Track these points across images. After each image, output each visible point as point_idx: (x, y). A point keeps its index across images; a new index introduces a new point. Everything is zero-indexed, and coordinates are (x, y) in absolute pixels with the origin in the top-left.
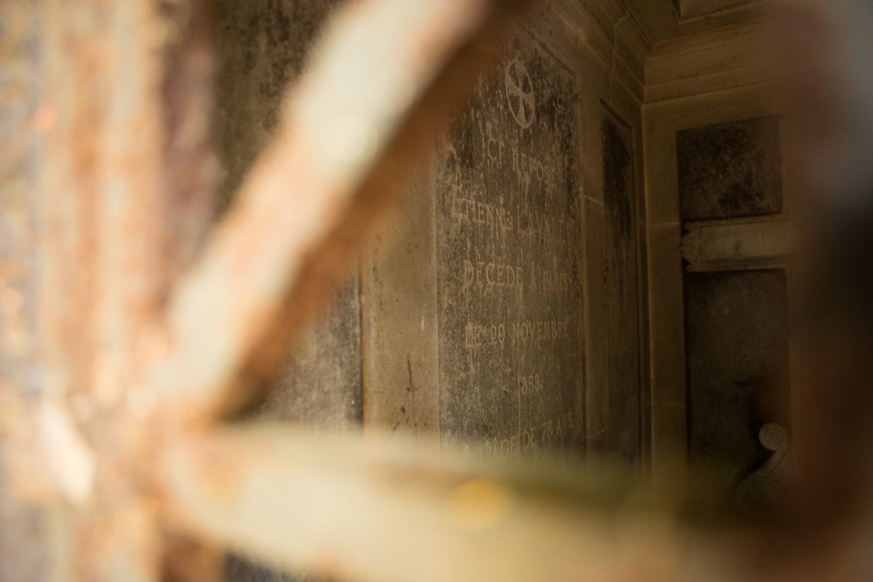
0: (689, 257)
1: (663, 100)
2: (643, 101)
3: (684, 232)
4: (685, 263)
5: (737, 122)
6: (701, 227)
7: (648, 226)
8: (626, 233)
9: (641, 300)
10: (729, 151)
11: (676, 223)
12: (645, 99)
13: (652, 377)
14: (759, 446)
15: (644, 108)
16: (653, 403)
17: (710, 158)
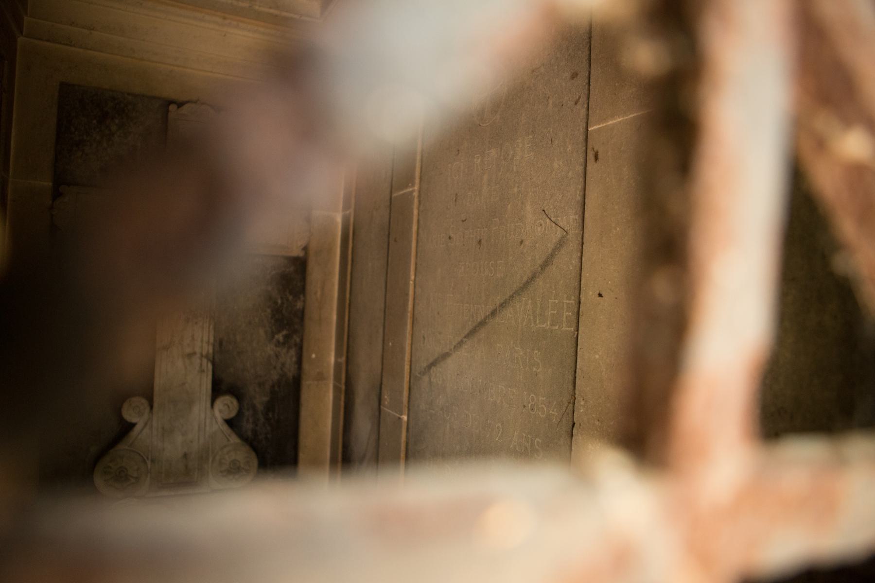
1: (48, 41)
2: (22, 33)
5: (129, 94)
10: (117, 121)
14: (121, 419)
15: (21, 40)
17: (95, 121)
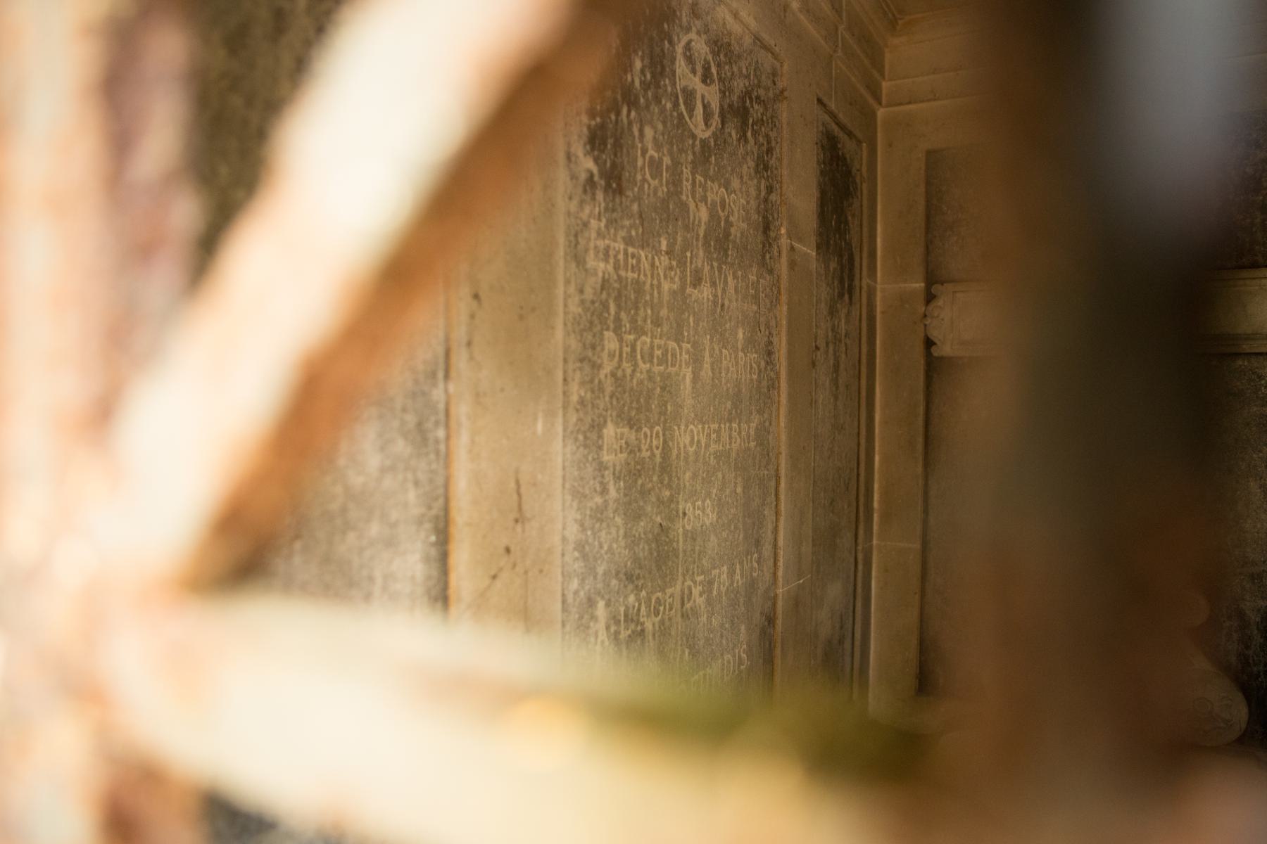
0: (935, 335)
1: (910, 103)
3: (930, 298)
4: (929, 343)
6: (955, 292)
7: (879, 287)
8: (846, 297)
9: (864, 393)
11: (920, 285)
12: (884, 102)
13: (876, 505)
15: (881, 113)
16: (875, 542)
